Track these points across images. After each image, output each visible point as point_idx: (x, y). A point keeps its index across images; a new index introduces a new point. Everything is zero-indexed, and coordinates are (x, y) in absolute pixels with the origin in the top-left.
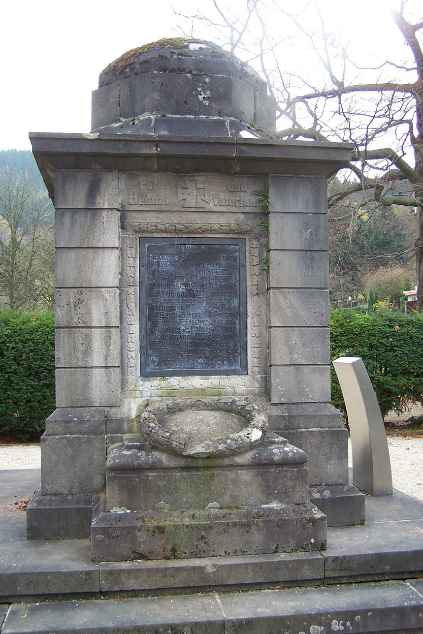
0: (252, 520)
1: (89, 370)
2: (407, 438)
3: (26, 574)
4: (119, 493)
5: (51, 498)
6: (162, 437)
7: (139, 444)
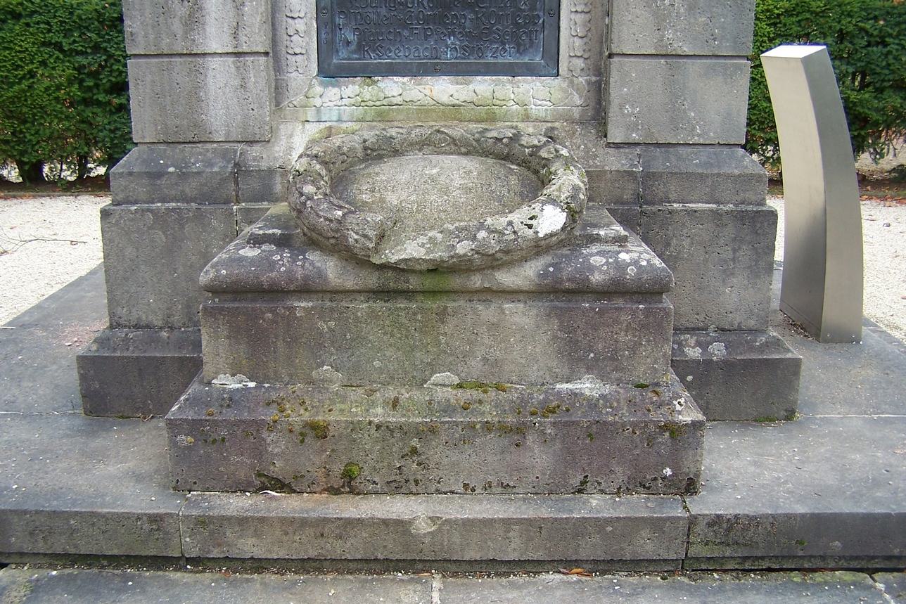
0: (529, 419)
1: (200, 60)
2: (887, 203)
3: (25, 512)
4: (230, 345)
5: (127, 335)
6: (326, 219)
7: (280, 232)
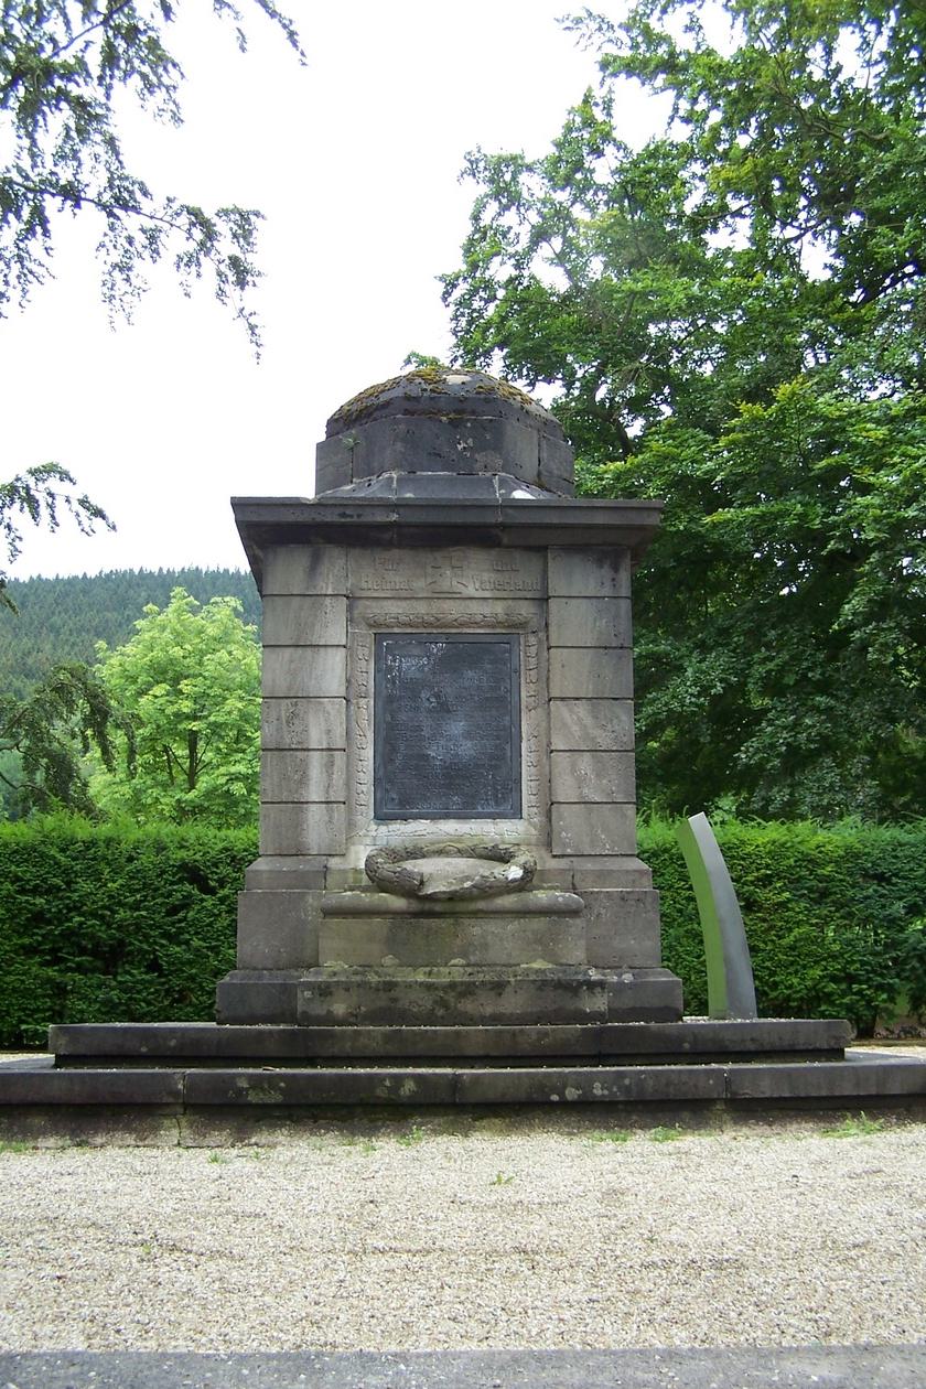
1: (305, 806)
